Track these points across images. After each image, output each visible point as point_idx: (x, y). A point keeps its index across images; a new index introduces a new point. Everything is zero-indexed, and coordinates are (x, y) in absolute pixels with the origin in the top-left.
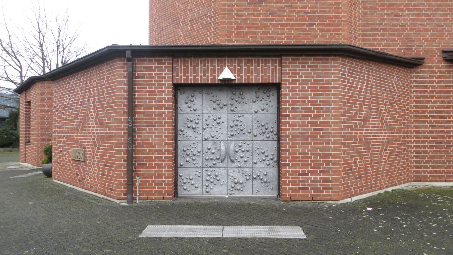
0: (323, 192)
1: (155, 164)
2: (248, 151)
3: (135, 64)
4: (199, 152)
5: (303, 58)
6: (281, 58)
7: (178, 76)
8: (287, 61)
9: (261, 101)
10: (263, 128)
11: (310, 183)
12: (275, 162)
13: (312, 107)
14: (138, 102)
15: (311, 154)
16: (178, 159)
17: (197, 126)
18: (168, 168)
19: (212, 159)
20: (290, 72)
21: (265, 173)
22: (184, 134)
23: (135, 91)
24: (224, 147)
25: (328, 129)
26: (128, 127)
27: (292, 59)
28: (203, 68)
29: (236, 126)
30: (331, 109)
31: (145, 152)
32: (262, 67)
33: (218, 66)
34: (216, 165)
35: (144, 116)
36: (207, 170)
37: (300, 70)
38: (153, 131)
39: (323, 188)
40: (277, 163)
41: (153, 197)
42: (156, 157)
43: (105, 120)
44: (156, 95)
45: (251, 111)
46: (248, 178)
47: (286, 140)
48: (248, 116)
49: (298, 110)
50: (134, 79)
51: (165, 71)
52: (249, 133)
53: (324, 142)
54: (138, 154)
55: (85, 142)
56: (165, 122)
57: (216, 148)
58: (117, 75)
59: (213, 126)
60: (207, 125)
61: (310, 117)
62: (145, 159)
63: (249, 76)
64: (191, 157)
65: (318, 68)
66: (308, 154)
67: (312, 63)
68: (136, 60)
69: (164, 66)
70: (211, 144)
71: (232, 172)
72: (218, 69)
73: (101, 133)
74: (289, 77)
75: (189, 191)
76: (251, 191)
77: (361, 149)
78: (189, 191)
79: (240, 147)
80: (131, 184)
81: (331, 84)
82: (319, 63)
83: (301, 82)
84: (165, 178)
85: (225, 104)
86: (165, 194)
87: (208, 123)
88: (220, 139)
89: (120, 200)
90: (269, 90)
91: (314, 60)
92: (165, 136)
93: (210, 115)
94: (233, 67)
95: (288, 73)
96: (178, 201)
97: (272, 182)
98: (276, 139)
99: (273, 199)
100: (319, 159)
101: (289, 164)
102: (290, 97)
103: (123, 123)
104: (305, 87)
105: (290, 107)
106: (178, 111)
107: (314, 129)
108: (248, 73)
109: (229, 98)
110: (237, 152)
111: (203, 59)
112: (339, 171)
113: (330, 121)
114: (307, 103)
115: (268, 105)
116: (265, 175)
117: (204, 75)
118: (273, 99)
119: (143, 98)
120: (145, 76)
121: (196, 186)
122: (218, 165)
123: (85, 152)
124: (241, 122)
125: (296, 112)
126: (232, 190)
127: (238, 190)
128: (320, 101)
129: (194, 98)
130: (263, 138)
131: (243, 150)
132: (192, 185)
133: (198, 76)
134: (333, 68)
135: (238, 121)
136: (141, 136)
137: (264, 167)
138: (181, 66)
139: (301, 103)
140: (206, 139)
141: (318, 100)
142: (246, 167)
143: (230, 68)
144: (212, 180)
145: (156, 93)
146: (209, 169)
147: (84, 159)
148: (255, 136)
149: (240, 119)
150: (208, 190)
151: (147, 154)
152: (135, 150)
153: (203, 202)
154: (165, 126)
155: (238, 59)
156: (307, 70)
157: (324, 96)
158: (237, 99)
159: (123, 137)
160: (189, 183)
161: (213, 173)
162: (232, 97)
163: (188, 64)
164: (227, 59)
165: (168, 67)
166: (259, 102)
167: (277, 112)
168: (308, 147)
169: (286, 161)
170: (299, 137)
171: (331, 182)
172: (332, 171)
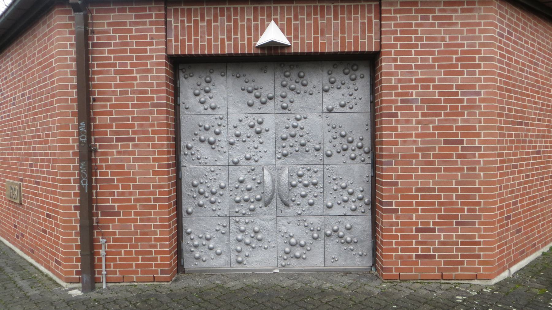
0: (462, 263)
1: (136, 214)
2: (315, 184)
3: (93, 18)
4: (222, 188)
7: (176, 40)
9: (339, 88)
10: (344, 140)
11: (437, 246)
12: (367, 204)
13: (442, 98)
14: (99, 93)
15: (440, 190)
16: (183, 201)
17: (218, 138)
18: (161, 220)
19: (246, 201)
20: (399, 29)
21: (348, 226)
22: (192, 154)
23: (93, 71)
24: (270, 178)
25: (473, 142)
26: (80, 142)
28: (226, 24)
29: (293, 136)
30: (479, 102)
31: (116, 191)
32: (343, 19)
33: (256, 19)
34: (254, 212)
35: (112, 120)
36: (237, 222)
37: (418, 25)
38: (131, 150)
39: (463, 256)
40: (370, 207)
41: (134, 276)
42: (137, 200)
44: (135, 79)
45: (321, 108)
46: (315, 235)
47: (390, 164)
48: (314, 119)
49: (414, 105)
50: (90, 48)
51: (150, 30)
52: (317, 150)
53: (465, 167)
54: (103, 194)
56: (154, 132)
57: (254, 180)
58: (58, 40)
59: (248, 137)
60: (238, 136)
61: (437, 119)
62: (116, 205)
63: (316, 40)
64: (207, 197)
65: (454, 21)
66: (433, 190)
67: (441, 11)
68: (93, 9)
69: (148, 20)
70: (245, 172)
71: (286, 224)
72: (256, 26)
74: (396, 39)
75: (204, 261)
76: (322, 260)
78: (204, 261)
79: (300, 176)
80: (88, 253)
81: (479, 52)
82: (456, 11)
83: (419, 49)
84: (156, 240)
85: (271, 95)
86: (156, 272)
87: (238, 132)
88: (261, 162)
89: (71, 283)
90: (355, 67)
92: (155, 160)
93: (242, 117)
94: (285, 22)
95: (395, 32)
96: (185, 283)
97: (361, 241)
98: (369, 161)
99: (361, 274)
100: (454, 200)
101: (396, 211)
102: (399, 79)
103: (72, 134)
104: (427, 60)
105: (399, 98)
106: (181, 110)
107: (446, 142)
108: (316, 32)
109: (278, 84)
110: (294, 186)
111: (225, 7)
112: (493, 223)
113: (477, 125)
114: (431, 90)
115: (352, 97)
116: (348, 229)
117: (229, 39)
119: (110, 86)
120: (112, 42)
121: (219, 251)
122: (258, 211)
123: (22, 188)
124: (302, 129)
125: (411, 108)
126: (285, 257)
127: (297, 258)
128: (458, 87)
129: (210, 85)
130: (344, 159)
131: (306, 182)
132: (211, 249)
133: (216, 40)
134: (482, 21)
135: (295, 127)
136: (106, 160)
137: (345, 215)
138: (182, 22)
139: (420, 90)
140: (236, 164)
141: (454, 84)
142: (313, 214)
143: (279, 23)
144: (248, 241)
145: (135, 75)
146: (242, 219)
147: (21, 201)
148: (329, 156)
149: (300, 124)
150: (240, 259)
151: (119, 194)
152: (96, 186)
153: (230, 284)
154: (153, 139)
155: (295, 5)
156: (433, 25)
157: (465, 76)
158: (293, 86)
159: (73, 161)
160: (204, 245)
161: (250, 226)
162: (284, 83)
163: (196, 16)
164: (272, 6)
165: (156, 23)
166: (336, 91)
167: (369, 110)
168: (433, 177)
169: (391, 204)
170: (416, 157)
171: (479, 243)
172: (481, 223)
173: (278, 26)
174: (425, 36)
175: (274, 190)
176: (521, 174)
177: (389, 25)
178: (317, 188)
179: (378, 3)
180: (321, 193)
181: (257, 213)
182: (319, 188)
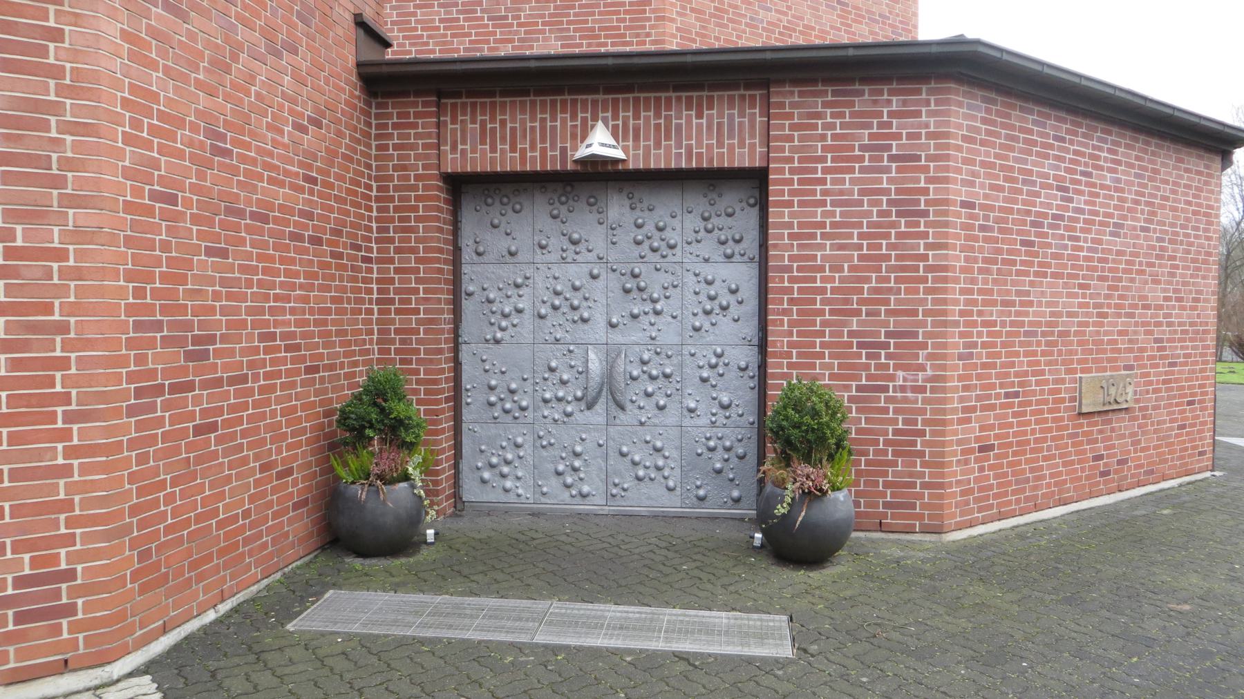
5: (933, 85)
6: (769, 92)
8: (789, 98)
19: (559, 400)
27: (834, 93)
43: (1191, 291)
55: (1130, 350)
73: (1180, 324)
77: (342, 366)
91: (801, 94)
110: (634, 379)
118: (747, 221)
122: (579, 417)
143: (611, 123)
173: (608, 128)
174: (923, 141)
175: (602, 385)
176: (293, 307)
177: (781, 127)
178: (670, 382)
179: (765, 92)
180: (678, 390)
181: (576, 420)
182: (674, 382)
